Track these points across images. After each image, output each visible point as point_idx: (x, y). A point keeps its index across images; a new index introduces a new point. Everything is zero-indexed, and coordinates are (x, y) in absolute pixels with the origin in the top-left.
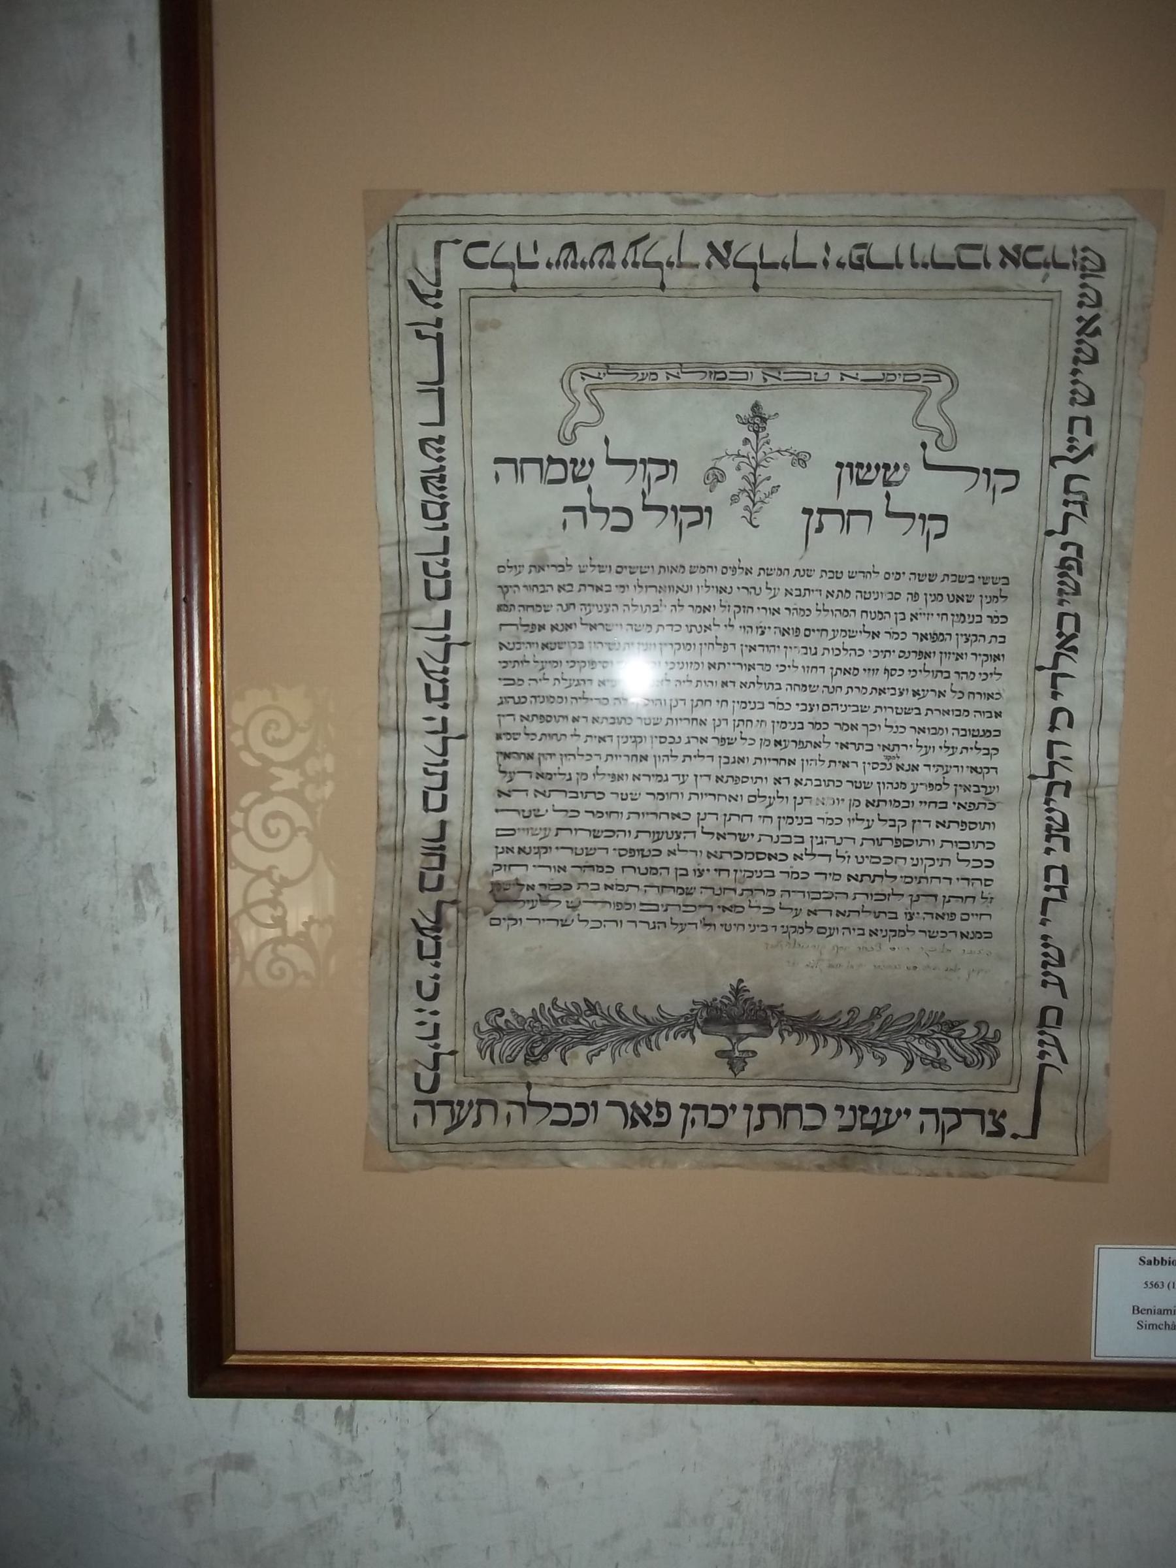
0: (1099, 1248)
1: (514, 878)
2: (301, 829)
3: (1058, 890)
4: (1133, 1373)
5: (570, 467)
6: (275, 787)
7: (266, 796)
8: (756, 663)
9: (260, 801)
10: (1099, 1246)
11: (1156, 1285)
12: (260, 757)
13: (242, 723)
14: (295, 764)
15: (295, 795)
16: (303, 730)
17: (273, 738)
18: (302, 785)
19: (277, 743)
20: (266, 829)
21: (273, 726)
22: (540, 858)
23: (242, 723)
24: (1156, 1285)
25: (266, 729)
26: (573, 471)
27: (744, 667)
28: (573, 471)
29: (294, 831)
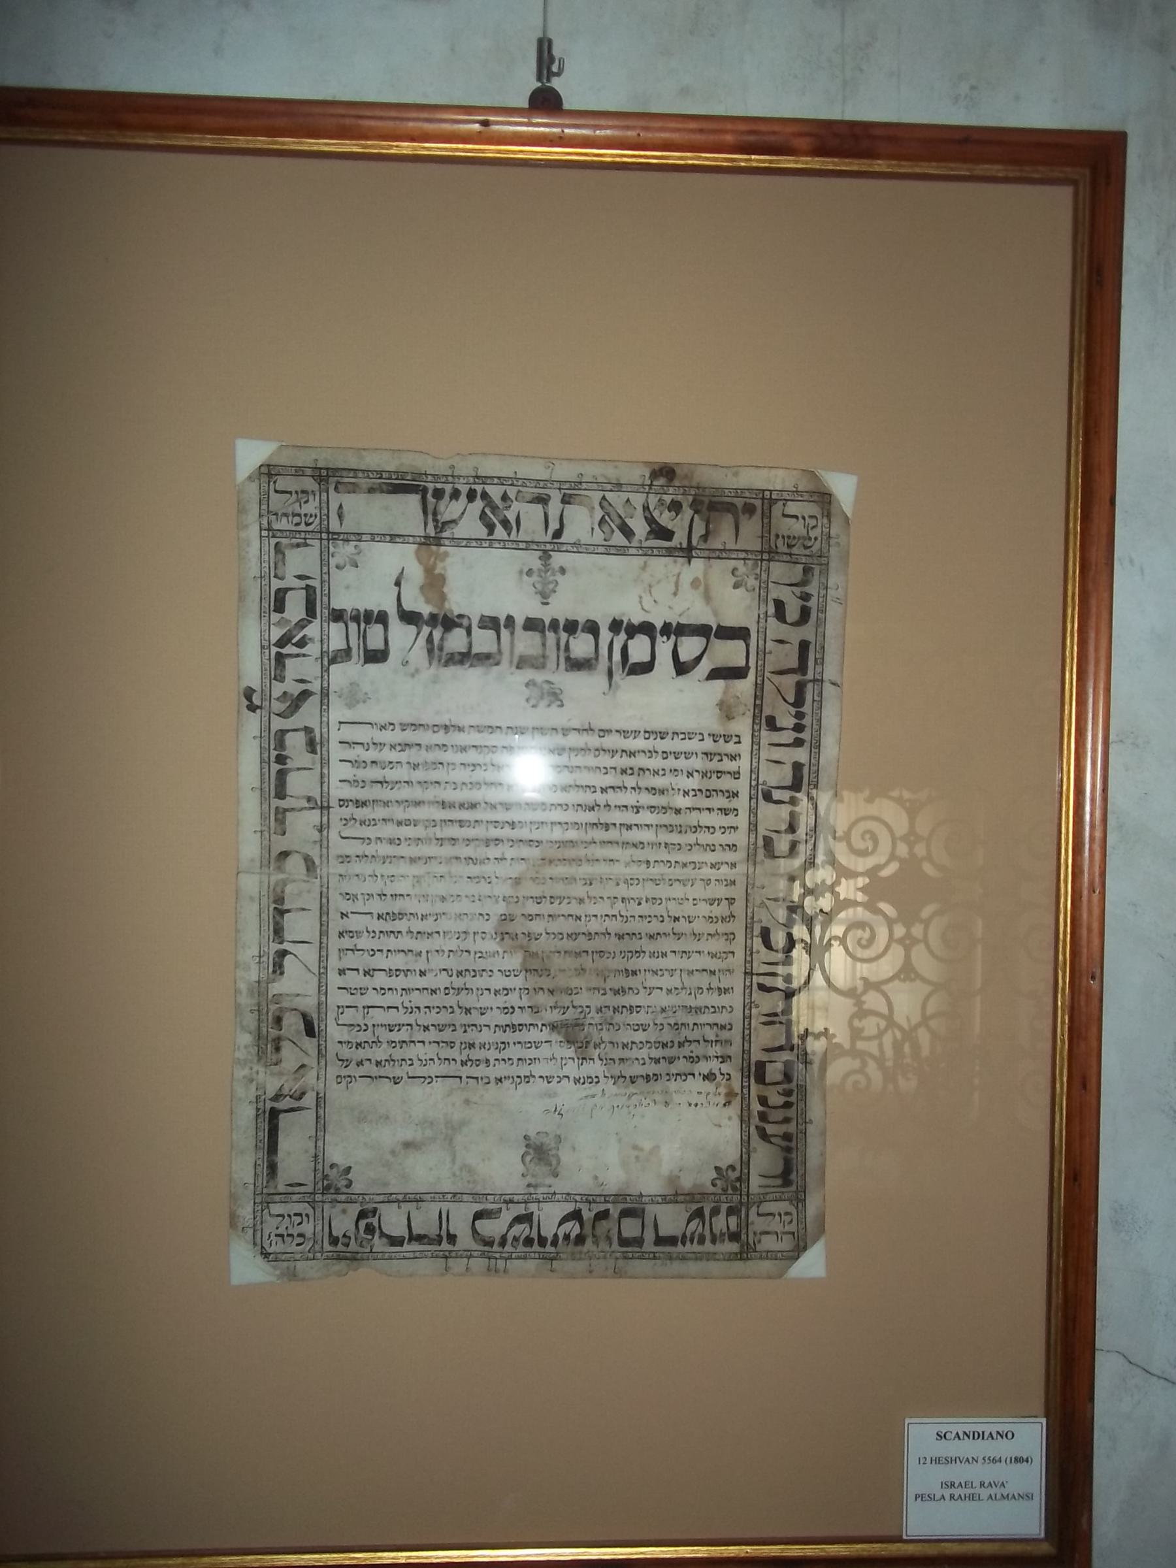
0: (1042, 1423)
1: (574, 774)
2: (840, 839)
3: (778, 726)
4: (989, 1549)
5: (303, 518)
6: (861, 881)
7: (872, 873)
8: (349, 911)
9: (879, 867)
10: (1044, 1424)
13: (894, 945)
14: (843, 904)
15: (846, 873)
16: (836, 938)
17: (864, 930)
18: (837, 883)
19: (860, 925)
20: (876, 842)
21: (864, 942)
22: (372, 738)
23: (894, 945)
25: (872, 939)
26: (531, 1228)
27: (375, 726)
28: (531, 1228)
29: (847, 837)
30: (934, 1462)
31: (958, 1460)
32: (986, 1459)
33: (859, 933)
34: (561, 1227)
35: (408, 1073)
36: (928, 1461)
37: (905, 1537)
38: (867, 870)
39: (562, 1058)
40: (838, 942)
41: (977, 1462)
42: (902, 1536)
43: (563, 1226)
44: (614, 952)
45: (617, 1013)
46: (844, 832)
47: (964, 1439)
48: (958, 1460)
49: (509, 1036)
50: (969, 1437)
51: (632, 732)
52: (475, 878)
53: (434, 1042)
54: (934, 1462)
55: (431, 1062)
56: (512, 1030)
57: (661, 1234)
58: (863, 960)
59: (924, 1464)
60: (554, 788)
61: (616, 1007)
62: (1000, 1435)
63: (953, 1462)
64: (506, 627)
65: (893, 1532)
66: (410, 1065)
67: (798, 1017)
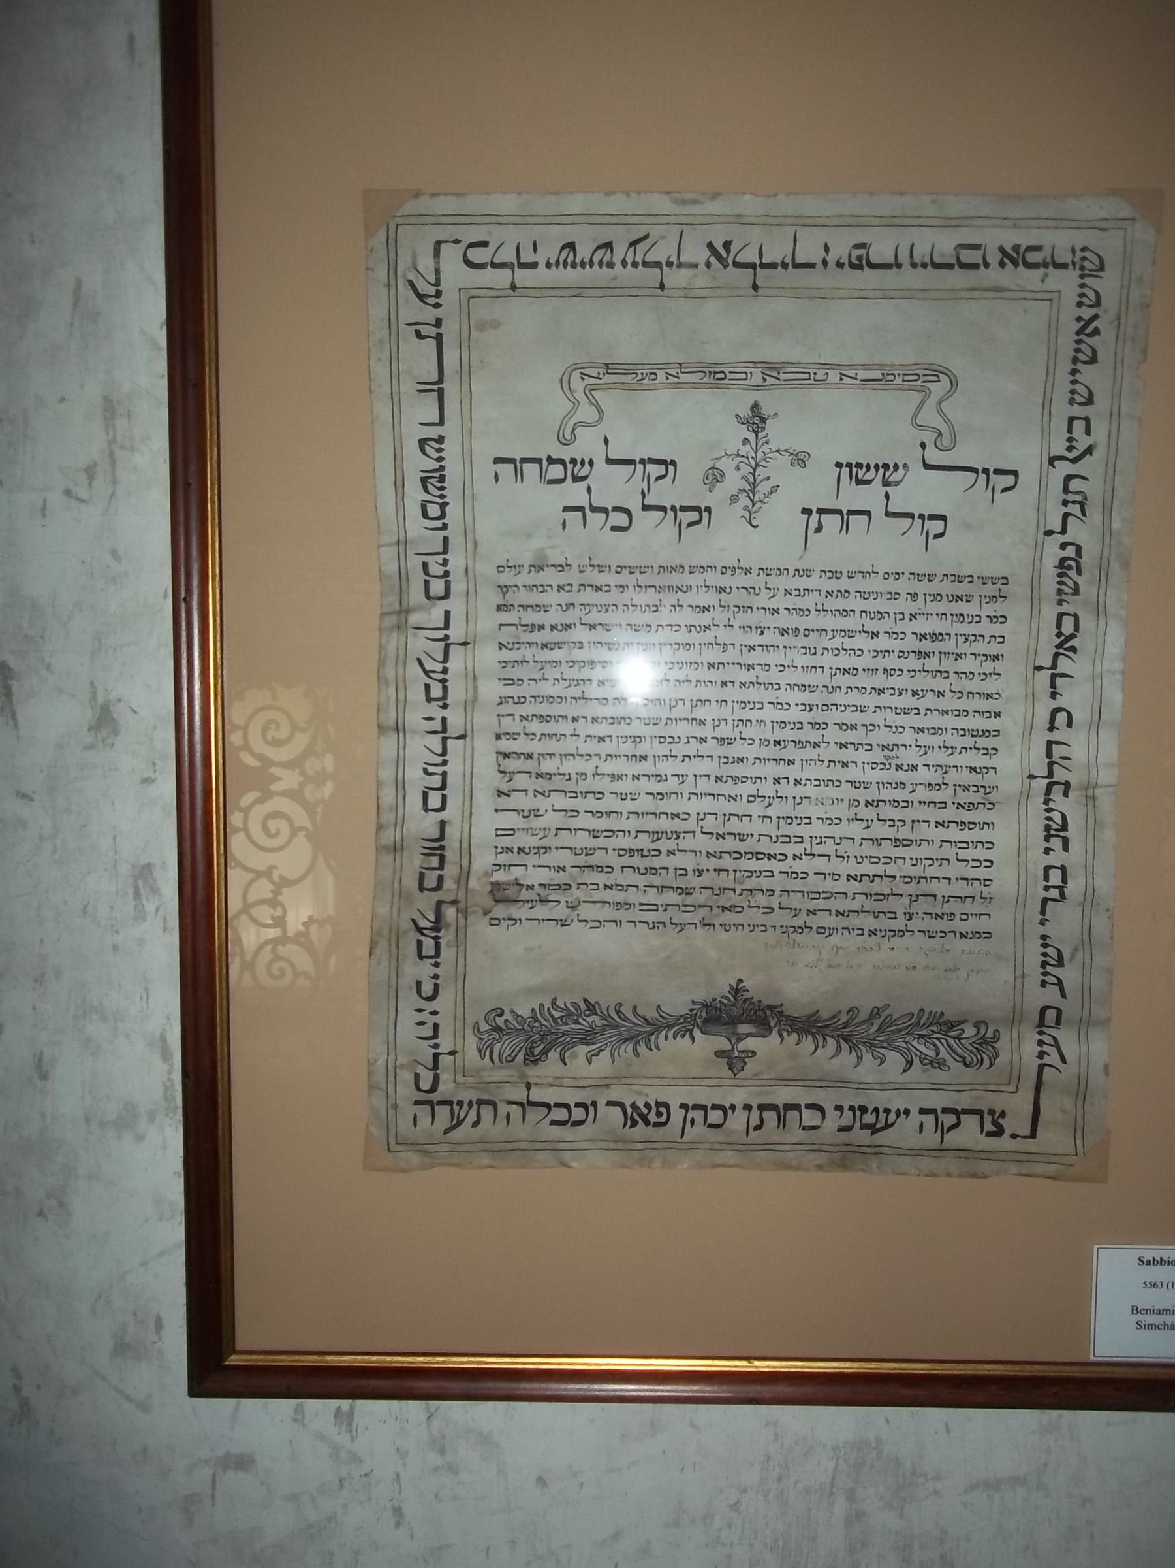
1: (514, 878)
2: (301, 829)
5: (570, 466)
6: (275, 787)
7: (267, 796)
9: (260, 801)
11: (1155, 1285)
12: (260, 757)
13: (242, 723)
14: (295, 764)
16: (303, 730)
17: (273, 738)
18: (302, 785)
19: (276, 743)
20: (265, 829)
21: (273, 726)
23: (242, 723)
24: (1155, 1285)
25: (265, 729)
29: (294, 831)
33: (277, 735)
38: (272, 797)
40: (300, 726)
44: (730, 587)
46: (296, 836)
49: (842, 680)
53: (684, 719)
56: (917, 657)
57: (1029, 1134)
58: (268, 707)
60: (604, 664)
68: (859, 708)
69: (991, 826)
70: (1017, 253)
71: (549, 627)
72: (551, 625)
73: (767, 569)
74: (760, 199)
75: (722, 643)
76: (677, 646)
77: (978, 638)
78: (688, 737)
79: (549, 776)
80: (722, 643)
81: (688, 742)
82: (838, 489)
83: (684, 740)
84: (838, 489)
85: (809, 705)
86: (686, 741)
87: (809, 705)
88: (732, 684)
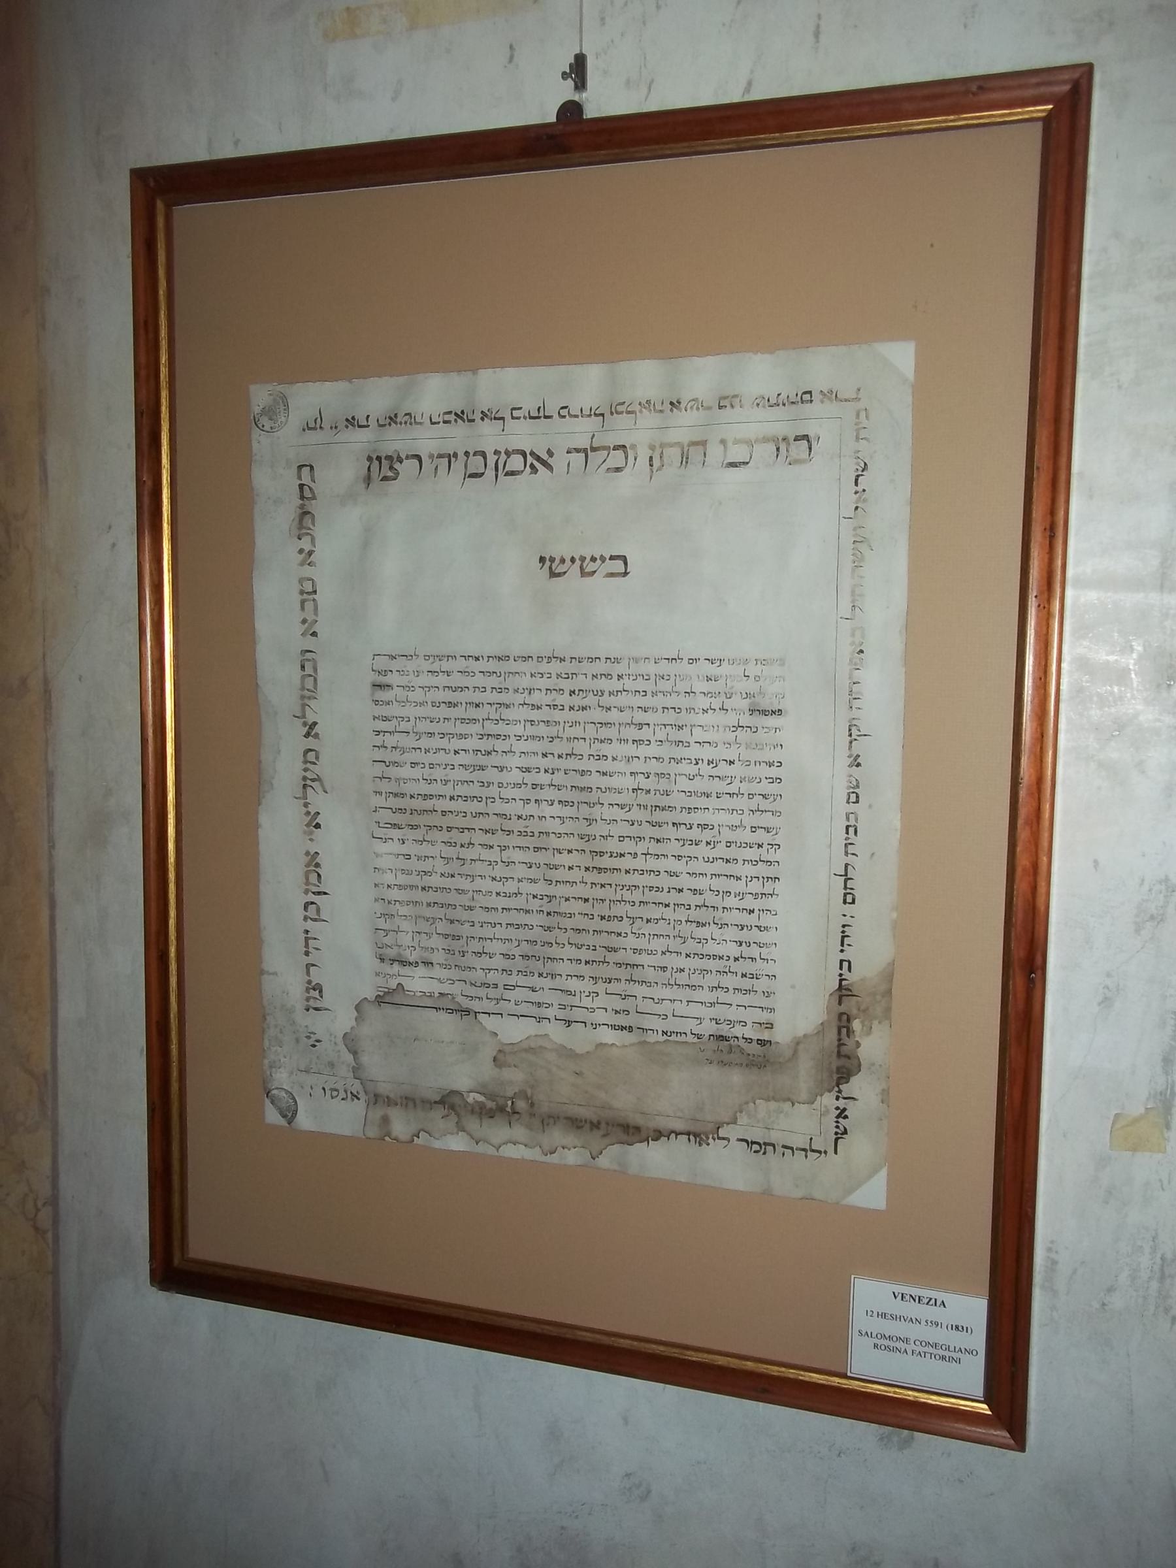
30: (880, 1317)
31: (902, 1318)
32: (929, 1322)
34: (565, 570)
35: (580, 870)
36: (875, 1314)
37: (849, 1374)
39: (486, 798)
41: (920, 1323)
42: (847, 1374)
43: (562, 571)
45: (612, 696)
47: (899, 1293)
48: (902, 1318)
50: (915, 1300)
51: (573, 560)
52: (434, 672)
54: (880, 1317)
55: (435, 782)
59: (871, 1316)
61: (612, 691)
62: (913, 1298)
63: (898, 1320)
64: (453, 457)
65: (842, 1370)
66: (632, 906)
67: (1016, 921)
68: (755, 976)
69: (619, 871)
70: (532, 466)
71: (624, 871)
72: (626, 870)
73: (621, 805)
74: (615, 1146)
75: (812, 399)
76: (639, 839)
77: (464, 689)
78: (669, 888)
79: (402, 796)
80: (812, 399)
81: (669, 892)
82: (586, 463)
83: (666, 890)
84: (586, 463)
85: (647, 773)
86: (668, 890)
87: (647, 773)
88: (609, 886)
